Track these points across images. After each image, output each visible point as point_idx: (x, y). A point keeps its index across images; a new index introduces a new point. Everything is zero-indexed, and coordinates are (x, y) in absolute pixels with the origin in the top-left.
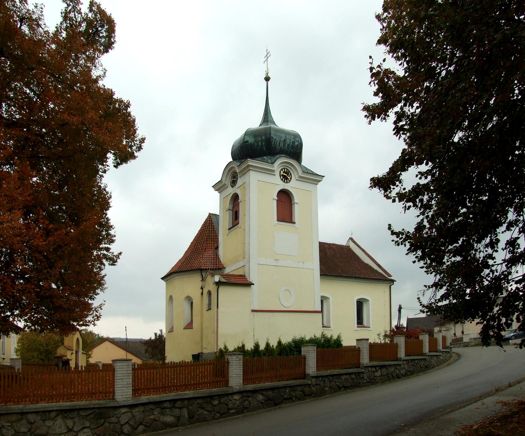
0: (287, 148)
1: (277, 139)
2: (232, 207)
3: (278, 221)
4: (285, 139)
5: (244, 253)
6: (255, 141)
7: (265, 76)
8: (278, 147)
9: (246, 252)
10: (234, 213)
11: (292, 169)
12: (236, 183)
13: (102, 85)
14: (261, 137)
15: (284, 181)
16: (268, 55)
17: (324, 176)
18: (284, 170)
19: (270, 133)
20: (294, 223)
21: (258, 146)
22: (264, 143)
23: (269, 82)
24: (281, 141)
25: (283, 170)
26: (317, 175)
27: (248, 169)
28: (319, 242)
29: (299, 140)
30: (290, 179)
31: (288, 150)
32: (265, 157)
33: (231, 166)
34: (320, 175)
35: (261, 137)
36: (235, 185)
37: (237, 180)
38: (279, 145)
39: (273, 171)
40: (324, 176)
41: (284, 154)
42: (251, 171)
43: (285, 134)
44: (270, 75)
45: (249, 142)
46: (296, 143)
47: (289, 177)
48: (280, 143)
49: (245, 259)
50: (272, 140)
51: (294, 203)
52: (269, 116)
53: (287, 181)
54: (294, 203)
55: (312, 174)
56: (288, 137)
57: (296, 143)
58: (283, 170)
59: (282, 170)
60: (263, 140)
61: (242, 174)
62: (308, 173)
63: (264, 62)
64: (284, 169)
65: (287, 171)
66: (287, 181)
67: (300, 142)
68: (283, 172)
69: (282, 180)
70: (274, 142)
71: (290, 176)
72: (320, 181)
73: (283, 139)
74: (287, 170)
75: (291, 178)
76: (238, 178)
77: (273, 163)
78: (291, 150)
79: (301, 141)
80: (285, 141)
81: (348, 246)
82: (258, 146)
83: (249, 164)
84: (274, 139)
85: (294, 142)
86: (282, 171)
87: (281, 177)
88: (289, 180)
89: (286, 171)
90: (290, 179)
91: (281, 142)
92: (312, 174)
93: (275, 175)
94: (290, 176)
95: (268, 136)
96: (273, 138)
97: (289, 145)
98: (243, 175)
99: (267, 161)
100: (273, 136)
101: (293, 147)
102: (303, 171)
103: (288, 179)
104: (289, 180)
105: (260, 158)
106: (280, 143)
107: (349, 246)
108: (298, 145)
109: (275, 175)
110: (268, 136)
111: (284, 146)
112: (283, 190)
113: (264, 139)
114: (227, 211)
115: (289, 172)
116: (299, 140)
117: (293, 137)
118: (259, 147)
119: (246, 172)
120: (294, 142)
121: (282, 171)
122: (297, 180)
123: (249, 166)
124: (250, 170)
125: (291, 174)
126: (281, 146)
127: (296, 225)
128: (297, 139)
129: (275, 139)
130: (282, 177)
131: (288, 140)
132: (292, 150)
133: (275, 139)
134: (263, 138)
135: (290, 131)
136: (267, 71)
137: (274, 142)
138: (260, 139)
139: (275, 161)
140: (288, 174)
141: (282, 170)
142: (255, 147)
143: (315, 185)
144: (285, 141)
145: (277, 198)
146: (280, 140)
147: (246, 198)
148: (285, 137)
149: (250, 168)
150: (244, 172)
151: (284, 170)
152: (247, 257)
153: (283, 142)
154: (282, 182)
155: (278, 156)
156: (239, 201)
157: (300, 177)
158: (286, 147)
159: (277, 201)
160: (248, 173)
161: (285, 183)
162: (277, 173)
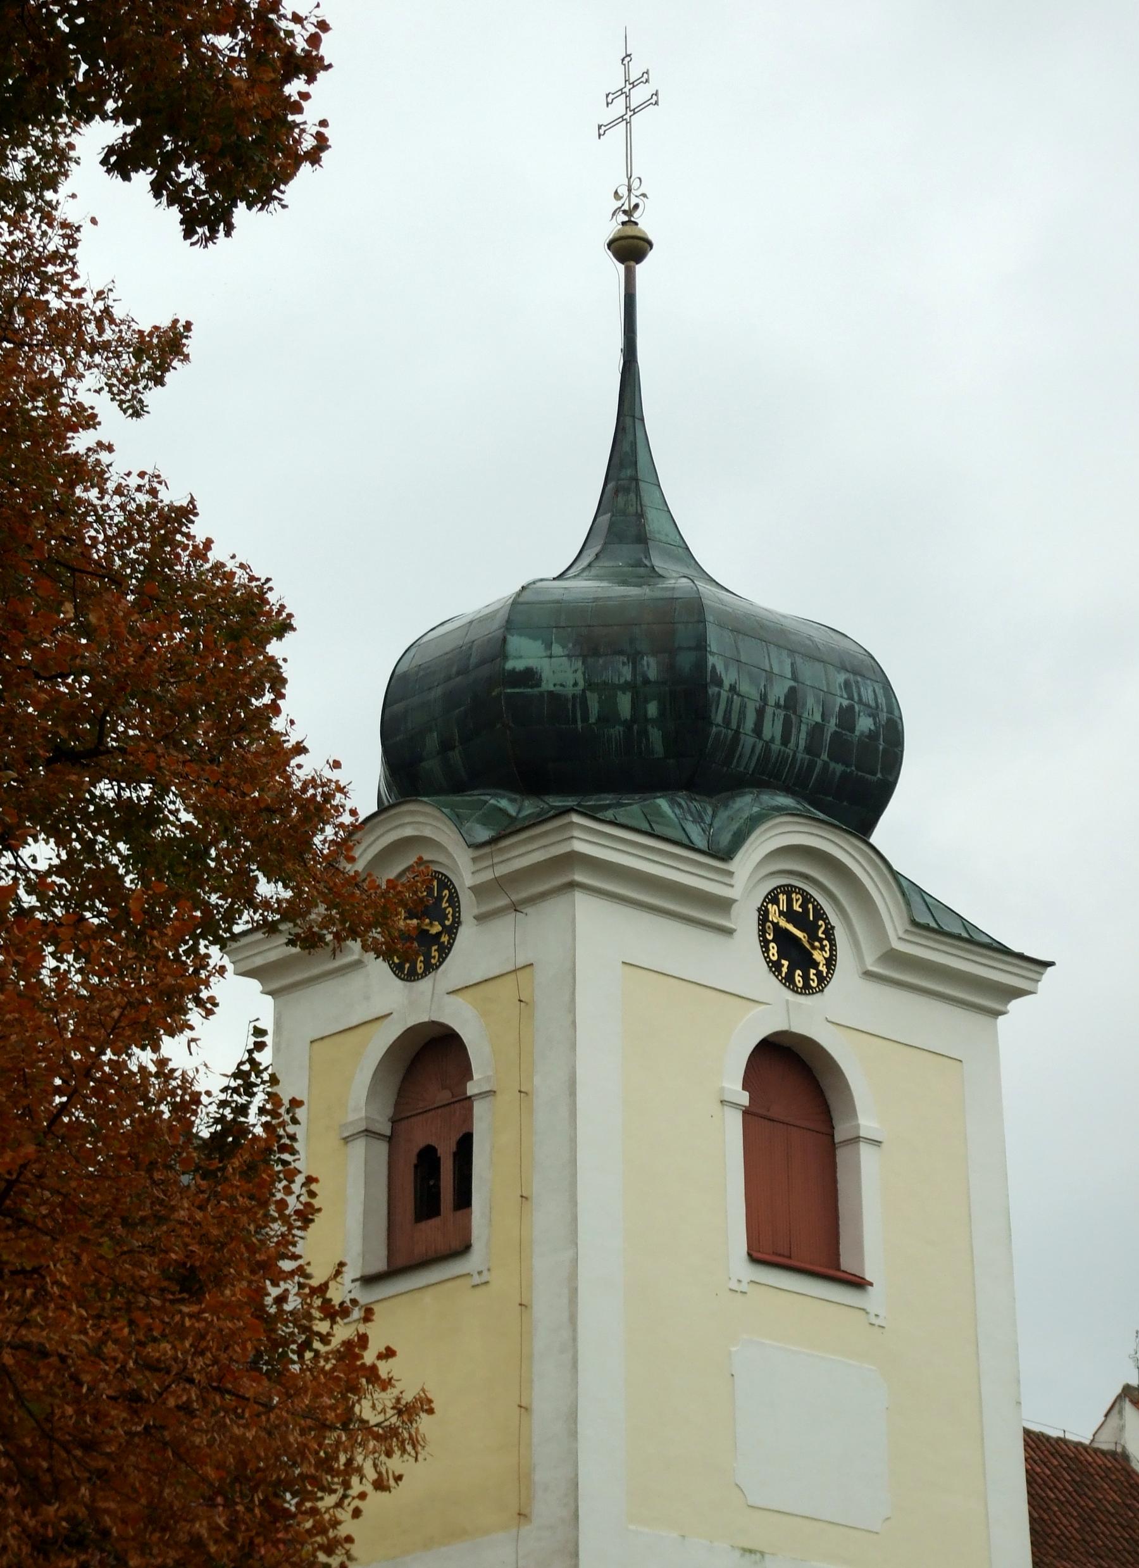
0: (808, 750)
1: (745, 687)
2: (390, 1111)
3: (755, 1258)
4: (792, 691)
5: (523, 1477)
6: (590, 685)
7: (612, 228)
8: (748, 741)
9: (540, 1476)
10: (409, 1158)
11: (849, 909)
12: (442, 959)
13: (200, 539)
14: (634, 659)
15: (788, 981)
16: (639, 95)
17: (1051, 964)
18: (790, 902)
19: (701, 646)
20: (858, 1283)
21: (608, 717)
22: (652, 709)
23: (640, 269)
24: (772, 701)
25: (782, 898)
26: (1003, 950)
27: (564, 880)
28: (1027, 1432)
29: (882, 700)
30: (824, 969)
31: (812, 765)
32: (663, 804)
33: (408, 832)
34: (1021, 956)
35: (634, 659)
36: (430, 968)
37: (452, 931)
38: (758, 730)
39: (724, 905)
40: (1051, 964)
41: (788, 790)
42: (579, 897)
43: (792, 652)
44: (647, 224)
45: (547, 686)
46: (864, 724)
47: (818, 956)
48: (760, 713)
49: (525, 1530)
50: (712, 690)
51: (859, 1137)
52: (646, 500)
53: (806, 978)
54: (856, 1139)
55: (971, 941)
56: (810, 673)
57: (864, 724)
58: (782, 898)
59: (775, 901)
60: (646, 681)
61: (502, 902)
62: (940, 932)
63: (601, 130)
64: (788, 890)
65: (806, 911)
66: (806, 978)
67: (883, 716)
68: (789, 915)
69: (775, 967)
70: (722, 706)
71: (822, 948)
72: (1019, 993)
73: (778, 691)
74: (807, 899)
75: (831, 962)
76: (457, 922)
77: (727, 855)
78: (832, 765)
79: (890, 710)
80: (792, 700)
81: (1113, 1454)
82: (608, 717)
83: (580, 847)
84: (726, 685)
85: (847, 717)
86: (772, 908)
87: (765, 945)
88: (819, 974)
89: (797, 907)
90: (824, 969)
91: (769, 711)
92: (971, 941)
93: (728, 932)
94: (822, 948)
95: (685, 661)
96: (719, 683)
97: (817, 730)
98: (515, 907)
99: (678, 835)
100: (720, 668)
101: (840, 746)
102: (914, 923)
103: (815, 964)
104: (819, 974)
105: (633, 810)
106: (760, 713)
107: (1125, 1457)
108: (873, 736)
109: (728, 932)
110: (685, 661)
111: (785, 741)
112: (786, 1042)
113: (652, 674)
114: (346, 1140)
115: (820, 914)
116: (882, 700)
117: (841, 678)
118: (617, 731)
119: (543, 896)
120: (847, 717)
121: (772, 908)
122: (868, 975)
123: (573, 859)
124: (572, 885)
125: (829, 932)
126: (767, 733)
127: (873, 1299)
128: (868, 695)
129: (733, 688)
130: (773, 949)
131: (810, 702)
132: (839, 768)
133: (733, 688)
134: (651, 667)
135: (787, 623)
136: (623, 191)
137: (722, 706)
138: (627, 673)
139: (739, 839)
140: (811, 929)
141: (775, 901)
142: (585, 718)
143: (982, 1020)
144: (792, 700)
145: (744, 1099)
146: (764, 698)
147: (537, 1080)
148: (794, 678)
149: (579, 878)
150: (524, 894)
151: (790, 902)
152: (546, 1508)
153: (781, 713)
154: (772, 987)
155: (745, 804)
156: (472, 1089)
157: (892, 957)
158: (802, 743)
159: (747, 1113)
160: (554, 908)
161: (795, 990)
162: (746, 922)
